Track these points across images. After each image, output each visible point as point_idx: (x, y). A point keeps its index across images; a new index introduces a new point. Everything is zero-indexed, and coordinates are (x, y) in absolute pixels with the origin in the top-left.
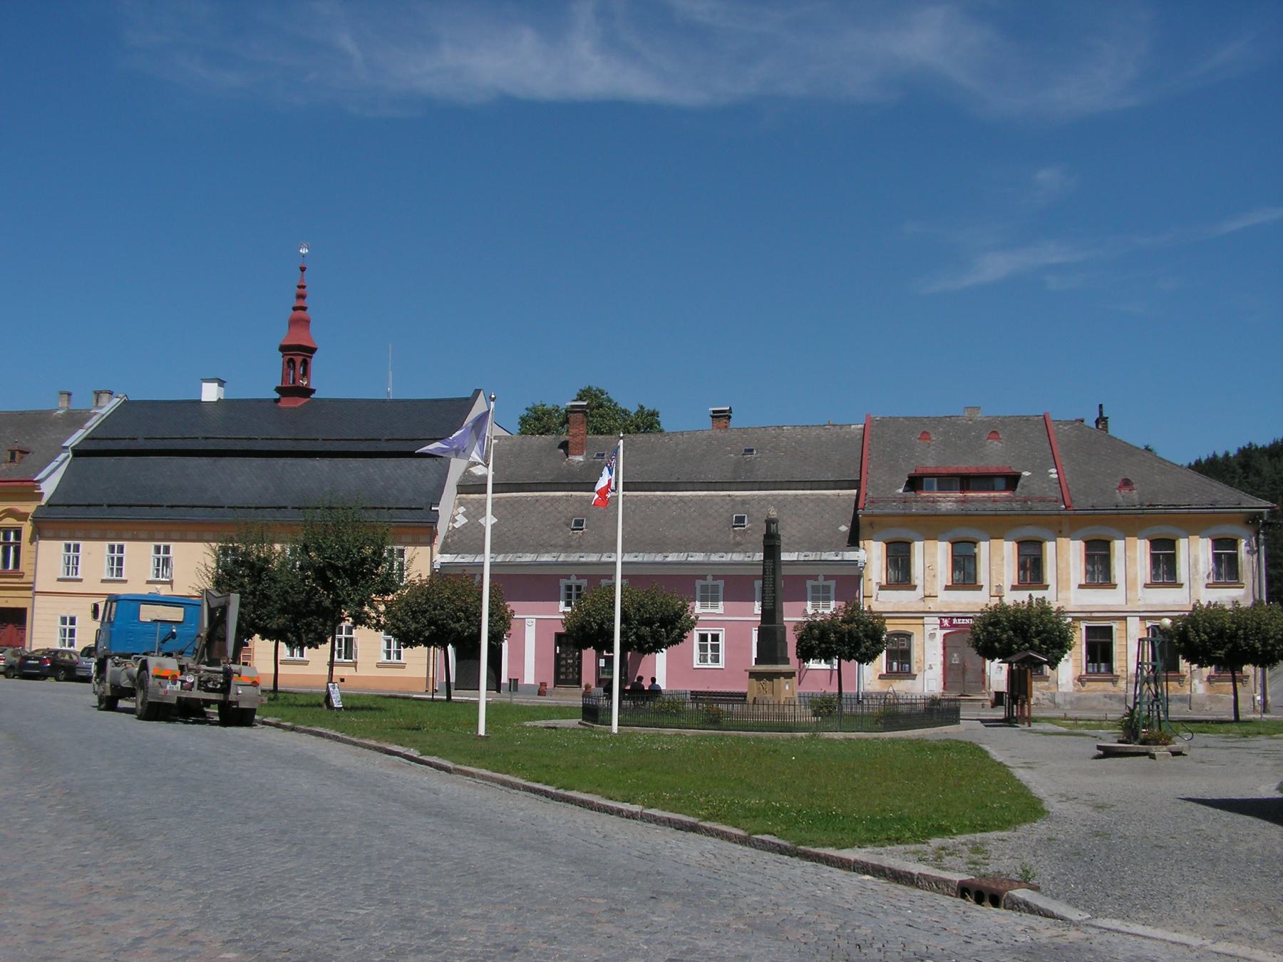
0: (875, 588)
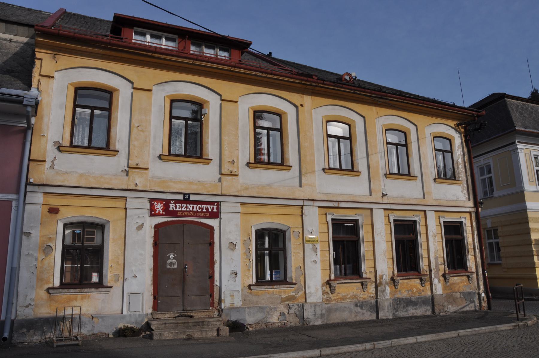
0: (51, 152)
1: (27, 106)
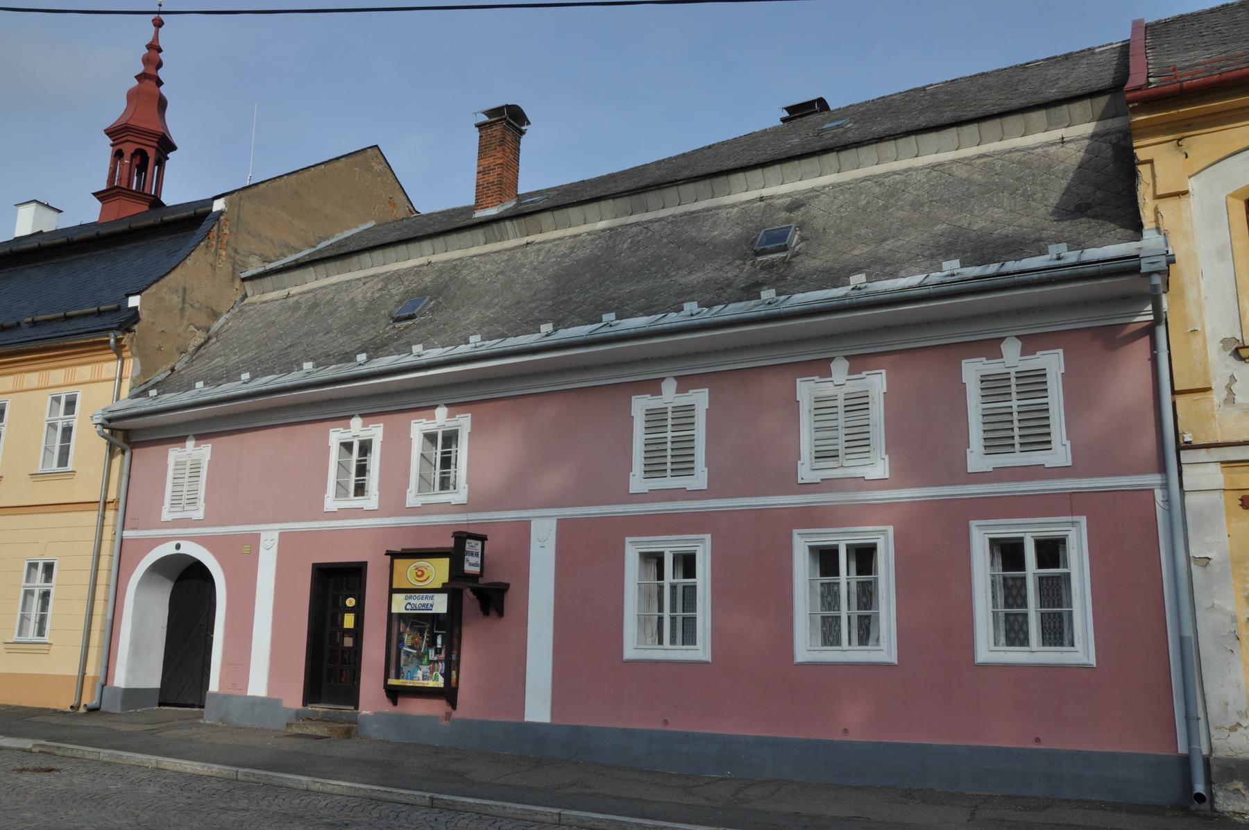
0: (1220, 366)
1: (1150, 274)
